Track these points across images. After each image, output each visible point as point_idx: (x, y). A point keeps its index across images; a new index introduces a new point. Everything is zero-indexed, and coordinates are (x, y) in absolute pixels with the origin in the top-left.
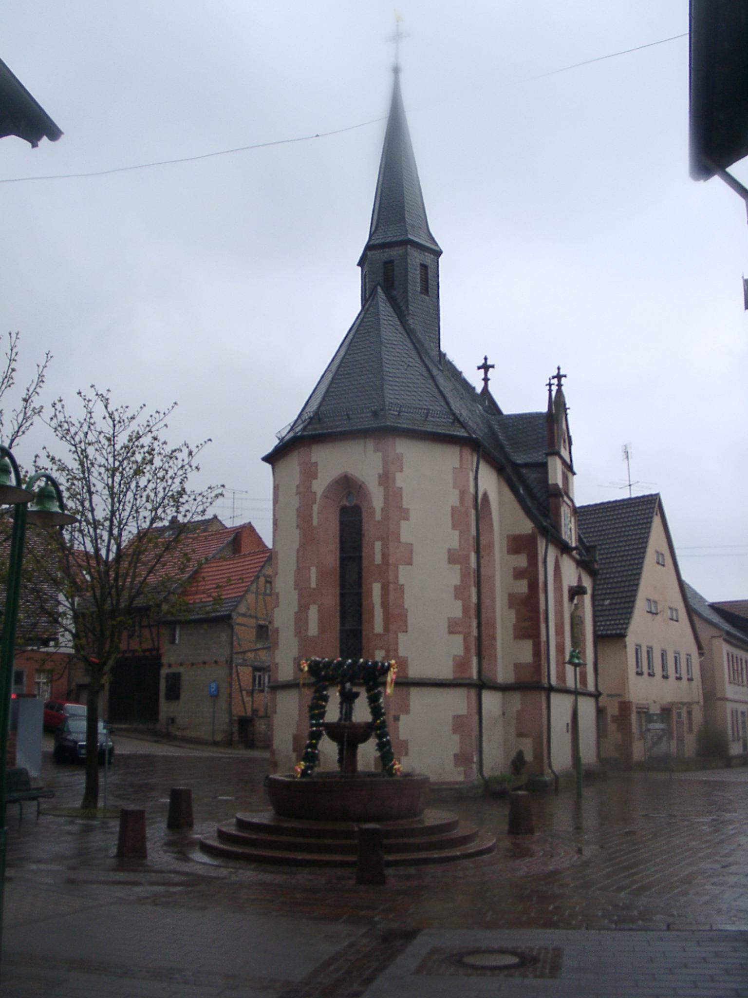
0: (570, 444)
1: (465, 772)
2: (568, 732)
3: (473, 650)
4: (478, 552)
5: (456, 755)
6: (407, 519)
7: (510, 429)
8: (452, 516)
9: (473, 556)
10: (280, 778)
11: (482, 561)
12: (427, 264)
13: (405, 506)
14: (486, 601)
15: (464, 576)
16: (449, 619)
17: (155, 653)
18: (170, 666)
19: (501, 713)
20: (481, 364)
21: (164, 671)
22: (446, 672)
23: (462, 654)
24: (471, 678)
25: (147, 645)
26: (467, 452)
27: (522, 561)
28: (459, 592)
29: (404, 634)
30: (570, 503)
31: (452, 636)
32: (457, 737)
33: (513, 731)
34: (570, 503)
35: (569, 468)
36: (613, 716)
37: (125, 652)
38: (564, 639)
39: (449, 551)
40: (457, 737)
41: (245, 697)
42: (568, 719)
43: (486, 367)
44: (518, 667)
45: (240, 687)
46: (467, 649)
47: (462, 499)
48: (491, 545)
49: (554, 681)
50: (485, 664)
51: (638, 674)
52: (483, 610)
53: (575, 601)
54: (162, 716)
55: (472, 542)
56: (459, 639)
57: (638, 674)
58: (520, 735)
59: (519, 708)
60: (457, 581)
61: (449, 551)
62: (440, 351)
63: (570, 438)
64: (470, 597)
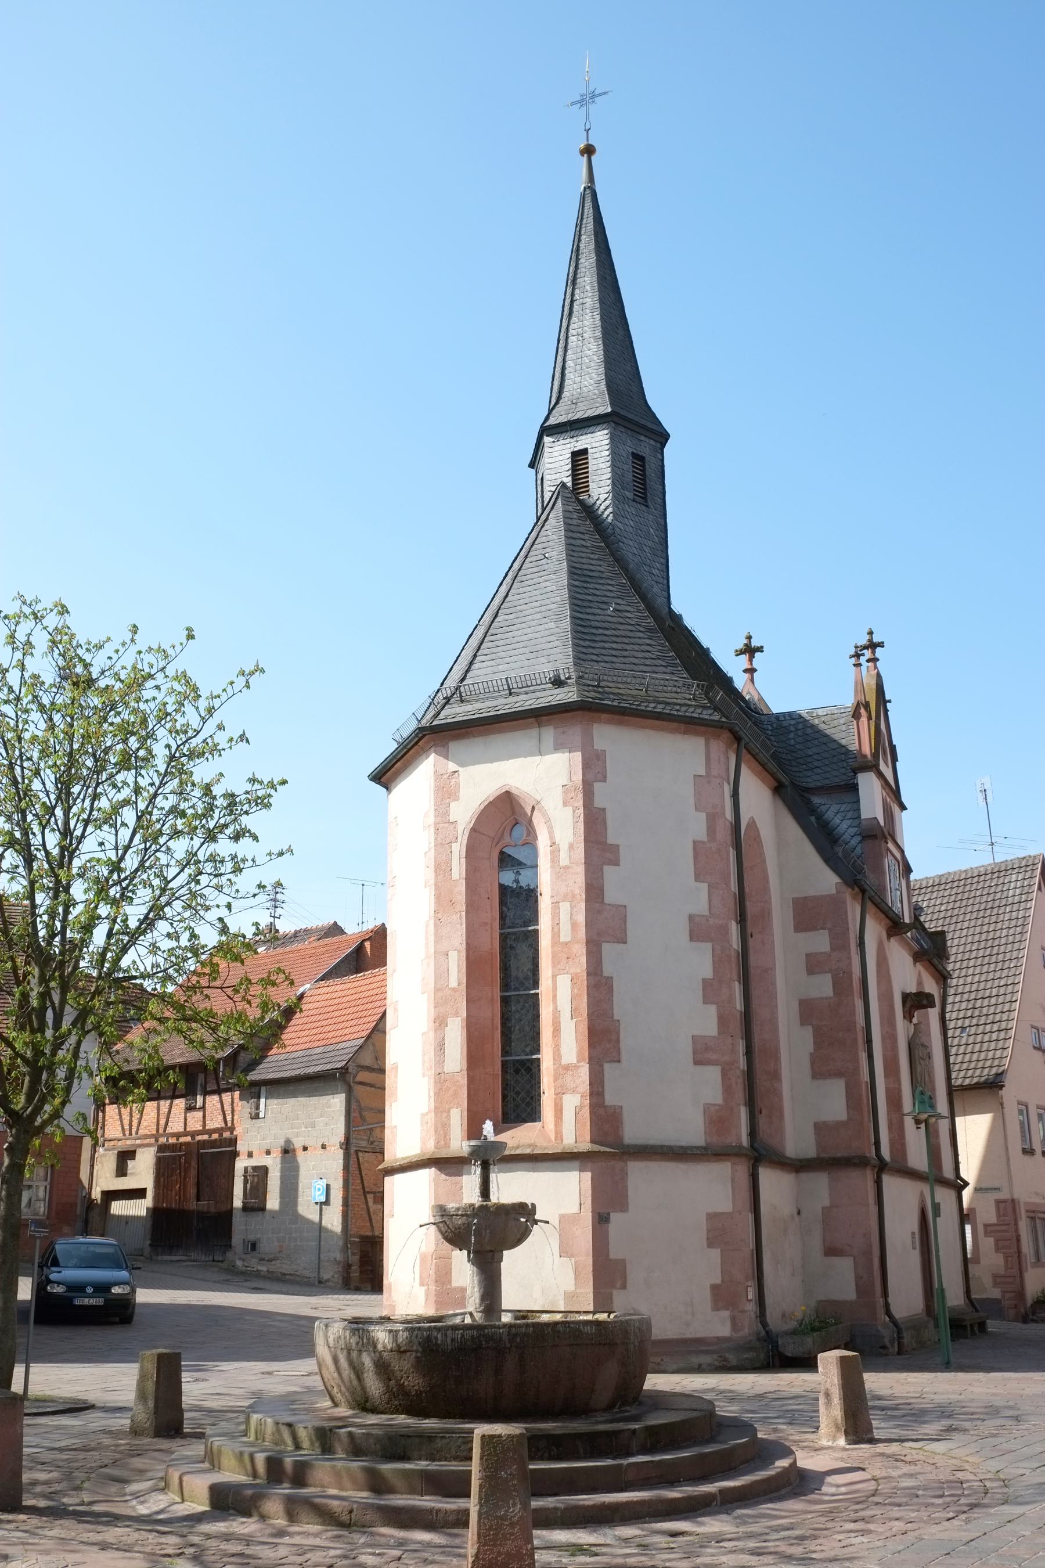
0: (895, 759)
1: (733, 1319)
2: (914, 1248)
3: (740, 1094)
4: (742, 920)
5: (714, 1288)
6: (616, 863)
7: (792, 735)
8: (695, 857)
9: (734, 929)
10: (764, 1437)
11: (751, 942)
12: (644, 455)
13: (611, 840)
14: (760, 1013)
15: (718, 963)
16: (695, 1039)
17: (226, 1135)
18: (250, 1155)
19: (795, 1211)
20: (740, 646)
21: (241, 1164)
22: (694, 1133)
23: (719, 1100)
24: (741, 1147)
25: (215, 1122)
26: (718, 747)
27: (820, 942)
28: (710, 990)
29: (615, 1065)
30: (898, 855)
31: (699, 1068)
32: (715, 1254)
33: (816, 1244)
34: (898, 855)
35: (894, 792)
36: (986, 1226)
37: (178, 1135)
38: (900, 1084)
39: (691, 918)
40: (715, 1254)
41: (371, 1204)
42: (914, 1225)
43: (750, 650)
44: (820, 1128)
45: (363, 1188)
46: (727, 1089)
47: (711, 830)
48: (765, 915)
49: (886, 1153)
50: (762, 1121)
51: (1025, 1151)
52: (756, 1030)
53: (915, 1020)
54: (237, 1239)
55: (731, 903)
56: (713, 1074)
57: (1025, 1151)
58: (831, 1251)
59: (827, 1203)
60: (707, 970)
61: (691, 918)
62: (671, 610)
63: (893, 749)
64: (731, 999)
